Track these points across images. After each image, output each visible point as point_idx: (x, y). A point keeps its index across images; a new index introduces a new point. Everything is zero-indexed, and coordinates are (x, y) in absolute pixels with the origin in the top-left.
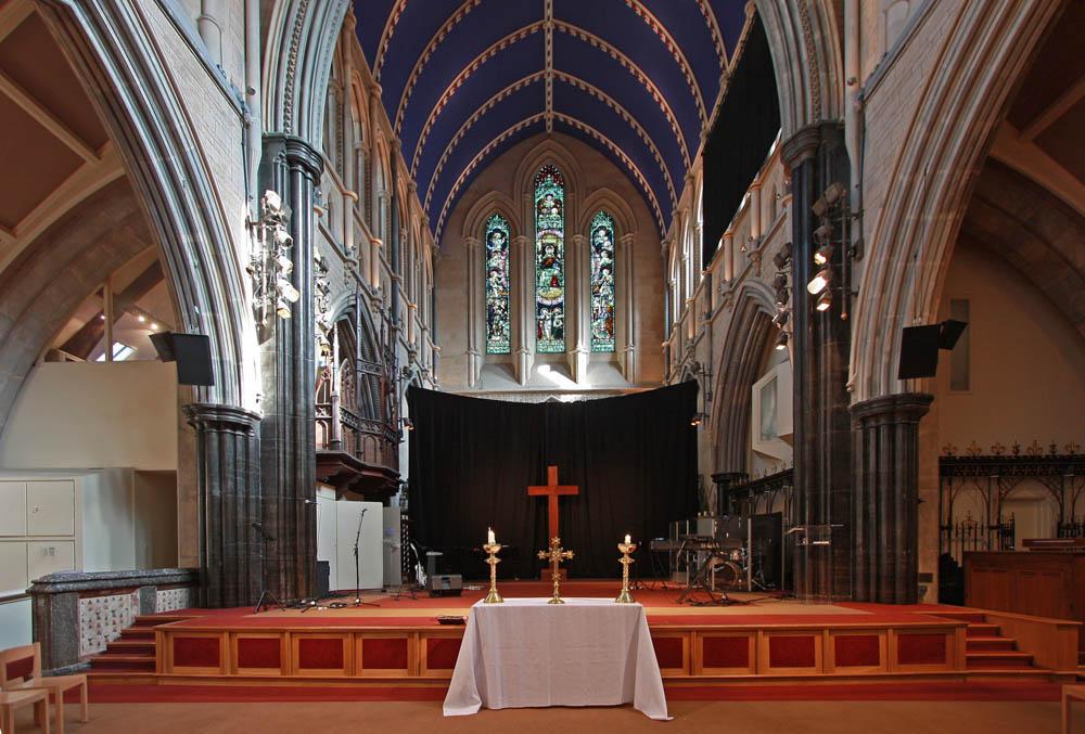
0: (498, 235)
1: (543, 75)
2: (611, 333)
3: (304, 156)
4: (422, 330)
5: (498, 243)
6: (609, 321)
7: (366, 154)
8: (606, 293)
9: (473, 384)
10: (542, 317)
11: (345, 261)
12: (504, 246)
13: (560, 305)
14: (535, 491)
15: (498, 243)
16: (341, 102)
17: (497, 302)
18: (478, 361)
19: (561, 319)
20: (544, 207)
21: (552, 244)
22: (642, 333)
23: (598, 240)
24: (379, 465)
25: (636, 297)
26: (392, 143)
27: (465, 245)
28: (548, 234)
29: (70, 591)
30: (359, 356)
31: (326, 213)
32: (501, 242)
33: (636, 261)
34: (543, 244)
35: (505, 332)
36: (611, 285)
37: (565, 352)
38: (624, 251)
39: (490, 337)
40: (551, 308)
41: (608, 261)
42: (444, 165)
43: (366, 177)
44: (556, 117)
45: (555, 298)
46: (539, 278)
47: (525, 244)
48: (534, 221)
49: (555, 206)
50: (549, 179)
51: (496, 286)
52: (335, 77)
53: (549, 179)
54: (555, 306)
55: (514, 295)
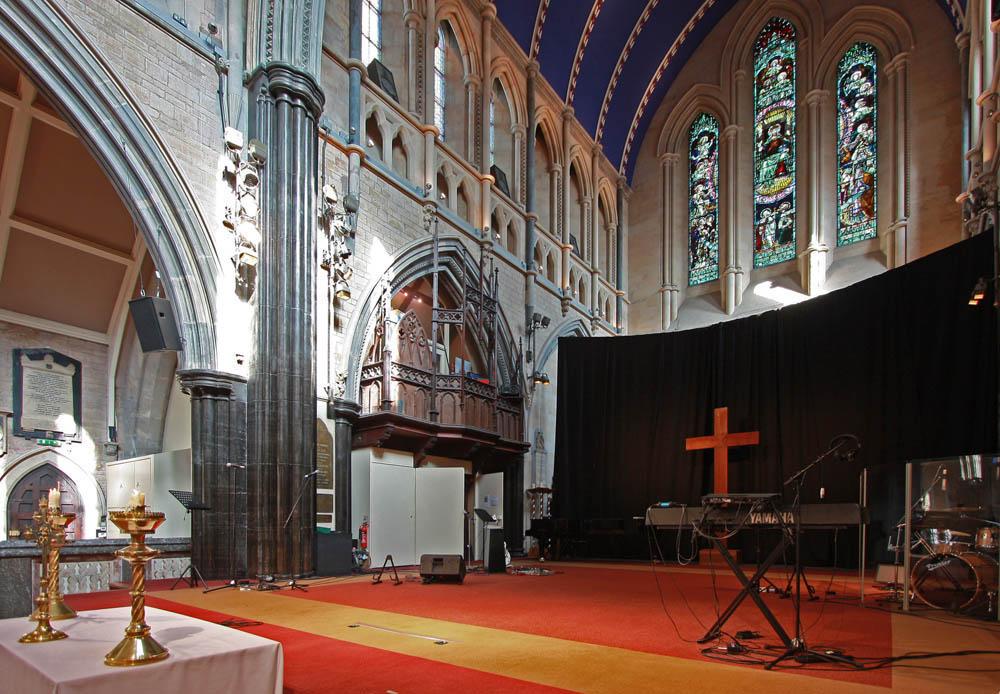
0: (706, 138)
2: (870, 212)
3: (287, 82)
4: (592, 274)
5: (704, 149)
6: (867, 196)
7: (476, 86)
11: (423, 204)
12: (711, 150)
13: (789, 198)
14: (695, 444)
17: (703, 221)
19: (791, 216)
21: (777, 122)
22: (922, 193)
24: (459, 425)
26: (528, 69)
27: (661, 165)
29: (21, 557)
35: (712, 254)
36: (872, 143)
37: (796, 258)
39: (693, 266)
40: (774, 206)
42: (581, 63)
45: (781, 191)
46: (758, 173)
47: (736, 135)
48: (753, 100)
49: (781, 71)
51: (701, 202)
54: (782, 201)
55: (721, 211)
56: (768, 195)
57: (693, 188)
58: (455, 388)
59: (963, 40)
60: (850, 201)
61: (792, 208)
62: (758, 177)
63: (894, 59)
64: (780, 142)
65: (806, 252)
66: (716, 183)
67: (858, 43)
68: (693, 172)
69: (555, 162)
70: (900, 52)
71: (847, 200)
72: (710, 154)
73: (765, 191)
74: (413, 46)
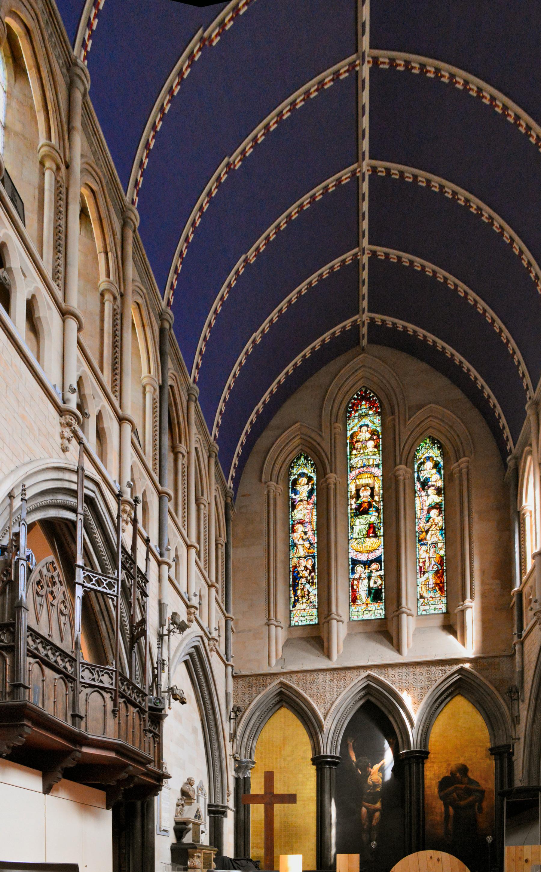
0: (304, 480)
1: (356, 255)
2: (441, 589)
5: (303, 489)
7: (115, 298)
8: (435, 539)
9: (273, 661)
10: (357, 576)
12: (311, 493)
13: (378, 560)
15: (303, 489)
16: (119, 311)
18: (280, 635)
19: (381, 577)
20: (358, 441)
21: (367, 485)
22: (483, 583)
23: (424, 475)
24: (111, 737)
25: (475, 538)
27: (266, 493)
28: (363, 472)
30: (80, 561)
31: (173, 564)
32: (307, 488)
33: (473, 492)
34: (356, 486)
38: (457, 482)
39: (294, 606)
40: (367, 564)
41: (438, 499)
43: (114, 332)
44: (374, 254)
45: (372, 551)
49: (370, 439)
50: (364, 405)
51: (301, 542)
52: (54, 141)
53: (364, 405)
54: (372, 561)
56: (361, 552)
57: (293, 526)
58: (107, 685)
59: (513, 461)
60: (426, 575)
61: (381, 569)
62: (352, 533)
63: (460, 461)
64: (370, 505)
65: (397, 613)
66: (315, 527)
67: (429, 437)
68: (293, 510)
69: (180, 442)
70: (464, 456)
71: (424, 573)
72: (309, 497)
73: (358, 548)
74: (50, 190)
